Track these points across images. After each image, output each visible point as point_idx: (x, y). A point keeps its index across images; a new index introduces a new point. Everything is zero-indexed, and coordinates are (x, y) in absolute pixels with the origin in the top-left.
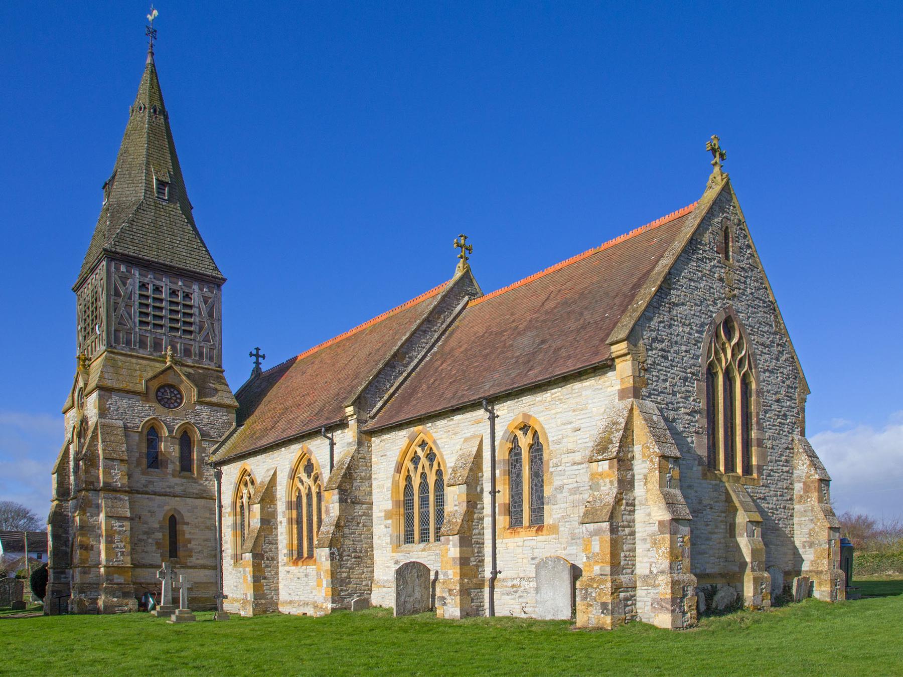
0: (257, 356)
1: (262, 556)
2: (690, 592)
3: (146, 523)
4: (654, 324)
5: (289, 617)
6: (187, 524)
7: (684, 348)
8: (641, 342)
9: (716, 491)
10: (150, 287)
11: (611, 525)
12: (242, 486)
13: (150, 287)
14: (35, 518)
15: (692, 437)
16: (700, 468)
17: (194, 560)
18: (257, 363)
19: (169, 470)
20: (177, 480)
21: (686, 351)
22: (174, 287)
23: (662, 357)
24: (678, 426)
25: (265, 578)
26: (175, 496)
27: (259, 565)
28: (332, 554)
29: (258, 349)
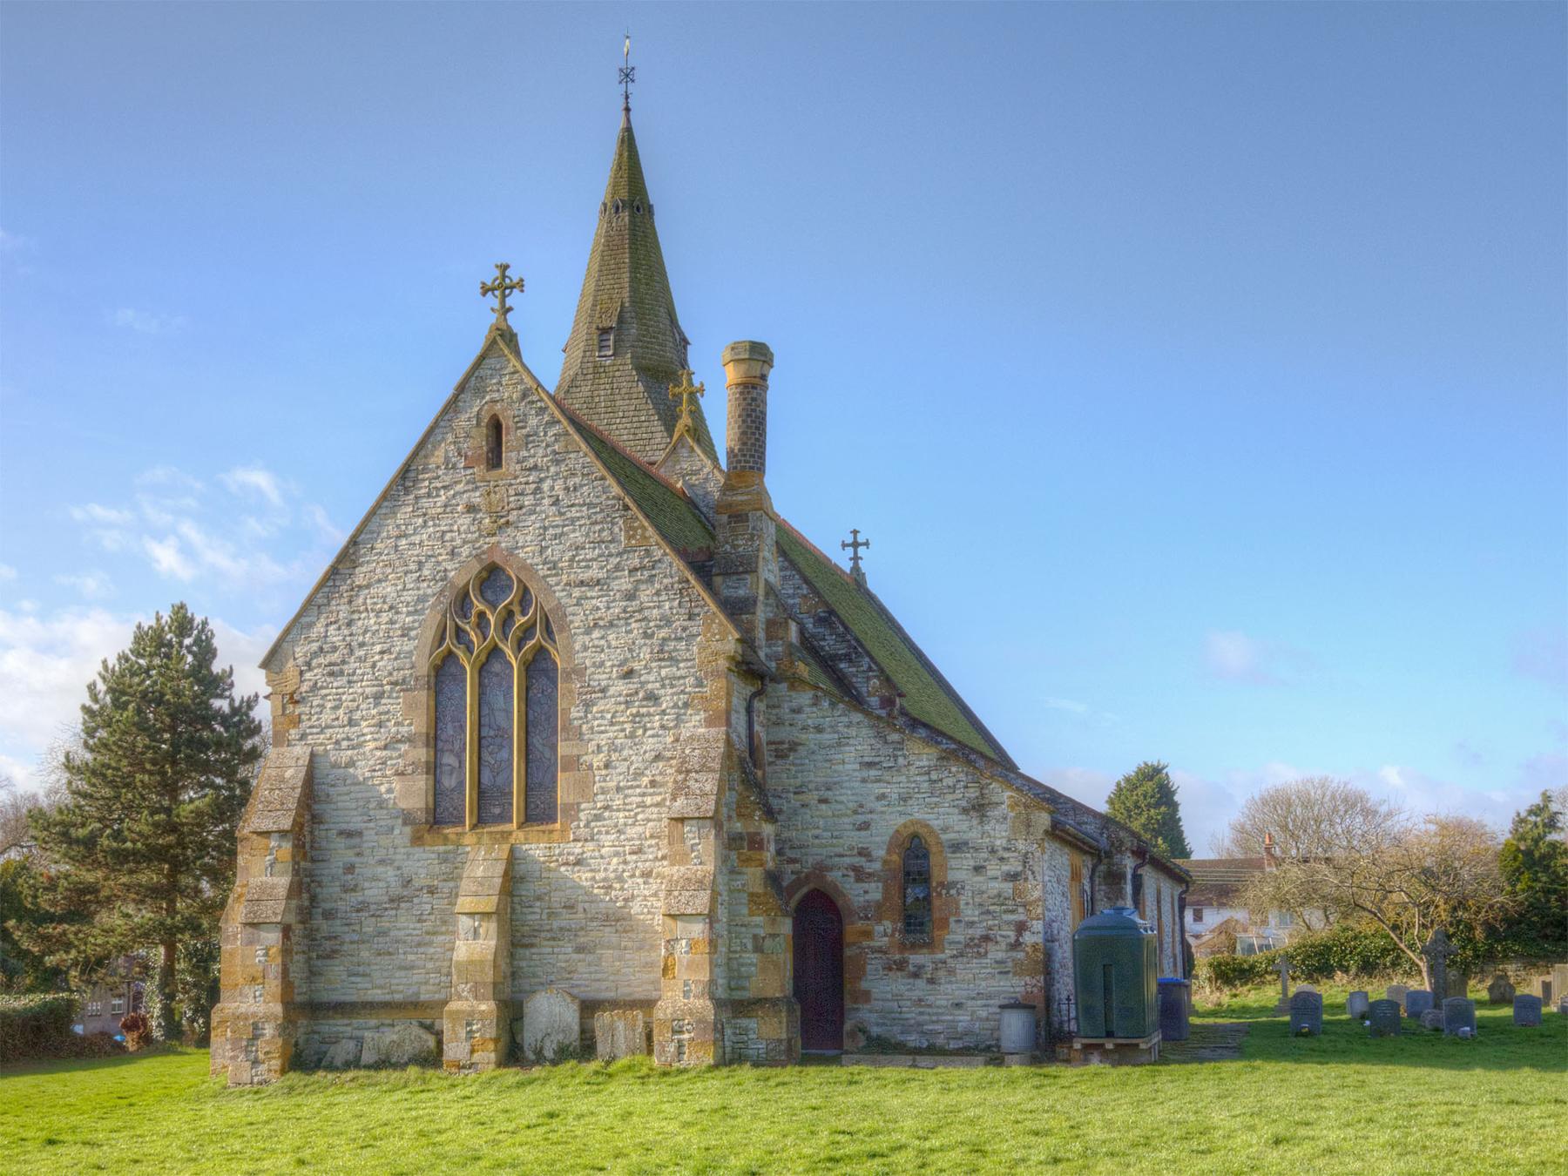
2: (269, 1031)
4: (319, 628)
7: (378, 648)
8: (291, 663)
9: (446, 861)
14: (1383, 809)
15: (390, 782)
16: (408, 829)
21: (382, 652)
23: (331, 674)
24: (359, 771)
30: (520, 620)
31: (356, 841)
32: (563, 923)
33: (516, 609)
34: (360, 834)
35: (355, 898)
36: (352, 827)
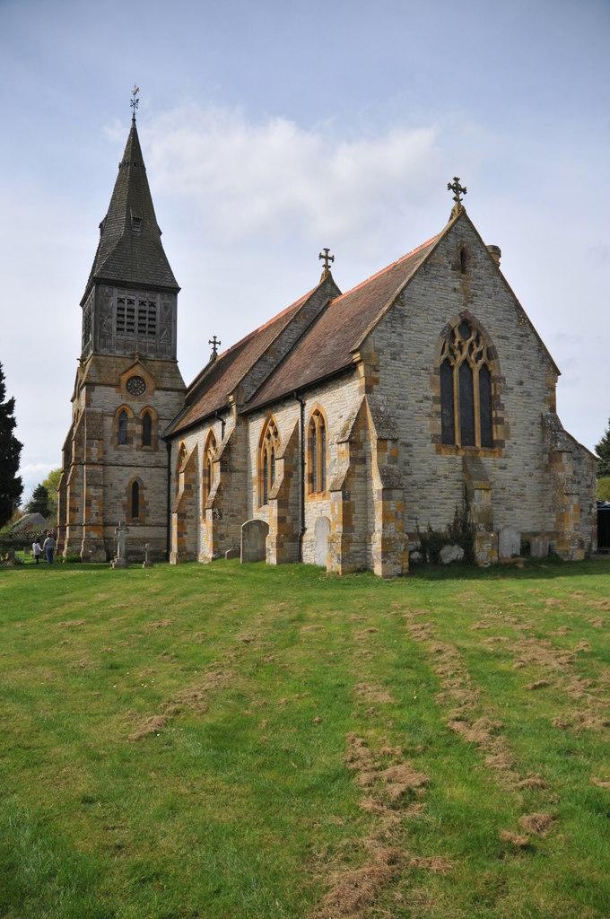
0: (215, 343)
1: (185, 514)
3: (116, 489)
5: (309, 566)
6: (146, 489)
10: (126, 301)
11: (343, 493)
12: (265, 439)
13: (126, 301)
17: (150, 519)
18: (215, 349)
19: (134, 446)
20: (140, 453)
22: (142, 299)
25: (186, 533)
26: (137, 466)
27: (183, 522)
28: (214, 513)
29: (215, 337)
30: (477, 350)
31: (410, 449)
32: (502, 496)
33: (475, 344)
34: (411, 445)
35: (410, 479)
36: (407, 441)
